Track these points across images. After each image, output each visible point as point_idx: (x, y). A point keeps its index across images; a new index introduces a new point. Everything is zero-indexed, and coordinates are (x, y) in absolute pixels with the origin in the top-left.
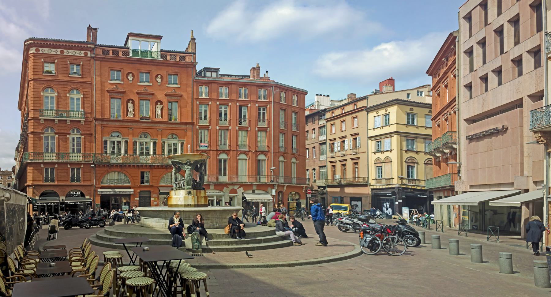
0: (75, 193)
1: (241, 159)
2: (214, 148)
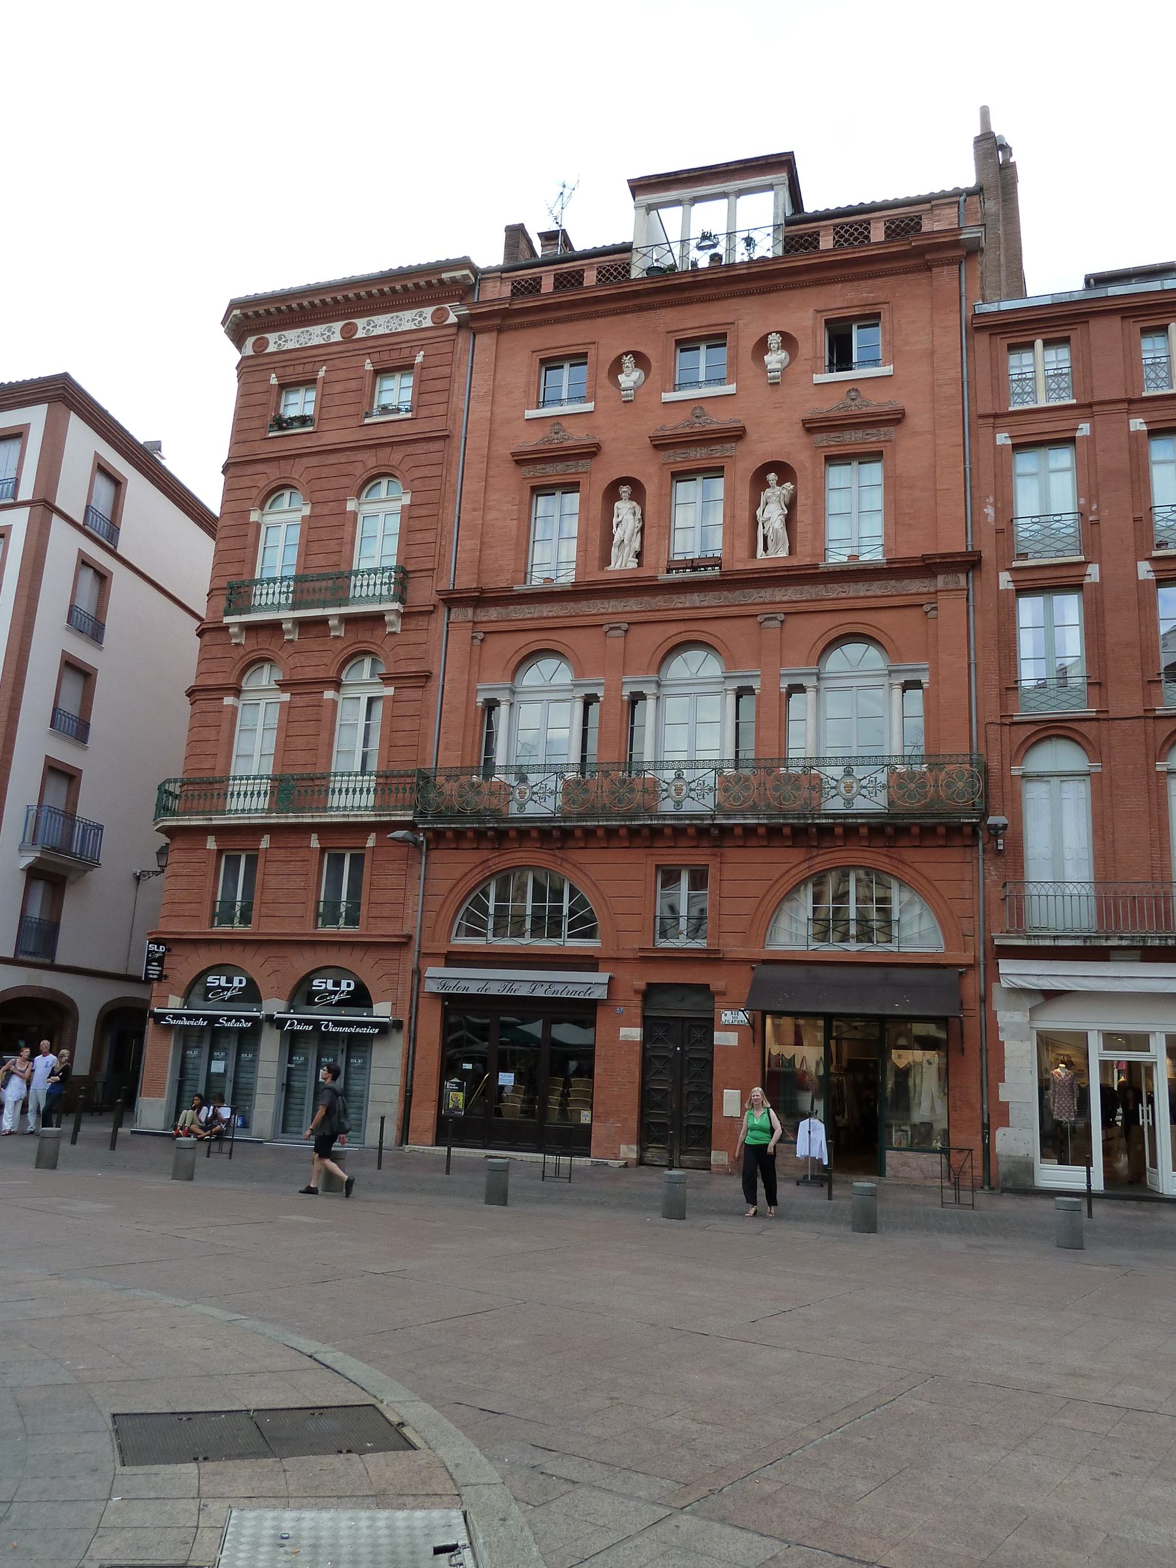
0: (330, 987)
1: (1040, 777)
2: (1126, 702)
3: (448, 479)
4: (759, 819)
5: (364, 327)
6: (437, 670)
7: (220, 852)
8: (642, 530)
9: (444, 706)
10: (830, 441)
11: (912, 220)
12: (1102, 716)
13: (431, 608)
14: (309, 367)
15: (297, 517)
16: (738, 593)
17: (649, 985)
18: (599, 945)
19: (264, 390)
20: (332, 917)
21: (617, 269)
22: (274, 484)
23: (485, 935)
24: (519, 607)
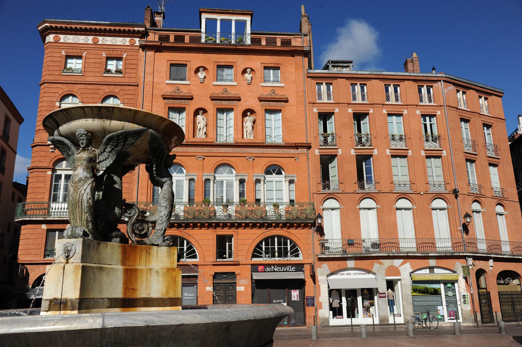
1: (327, 209)
3: (137, 100)
4: (250, 221)
5: (101, 40)
11: (288, 40)
12: (343, 192)
17: (215, 273)
19: (59, 56)
23: (262, 257)
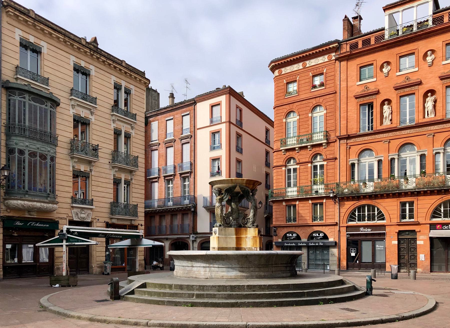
6: (338, 157)
7: (286, 205)
8: (392, 113)
9: (340, 166)
10: (402, 92)
13: (335, 141)
14: (294, 77)
15: (322, 114)
16: (420, 129)
18: (386, 222)
20: (290, 220)
21: (381, 36)
22: (289, 111)
23: (356, 221)
24: (359, 138)
